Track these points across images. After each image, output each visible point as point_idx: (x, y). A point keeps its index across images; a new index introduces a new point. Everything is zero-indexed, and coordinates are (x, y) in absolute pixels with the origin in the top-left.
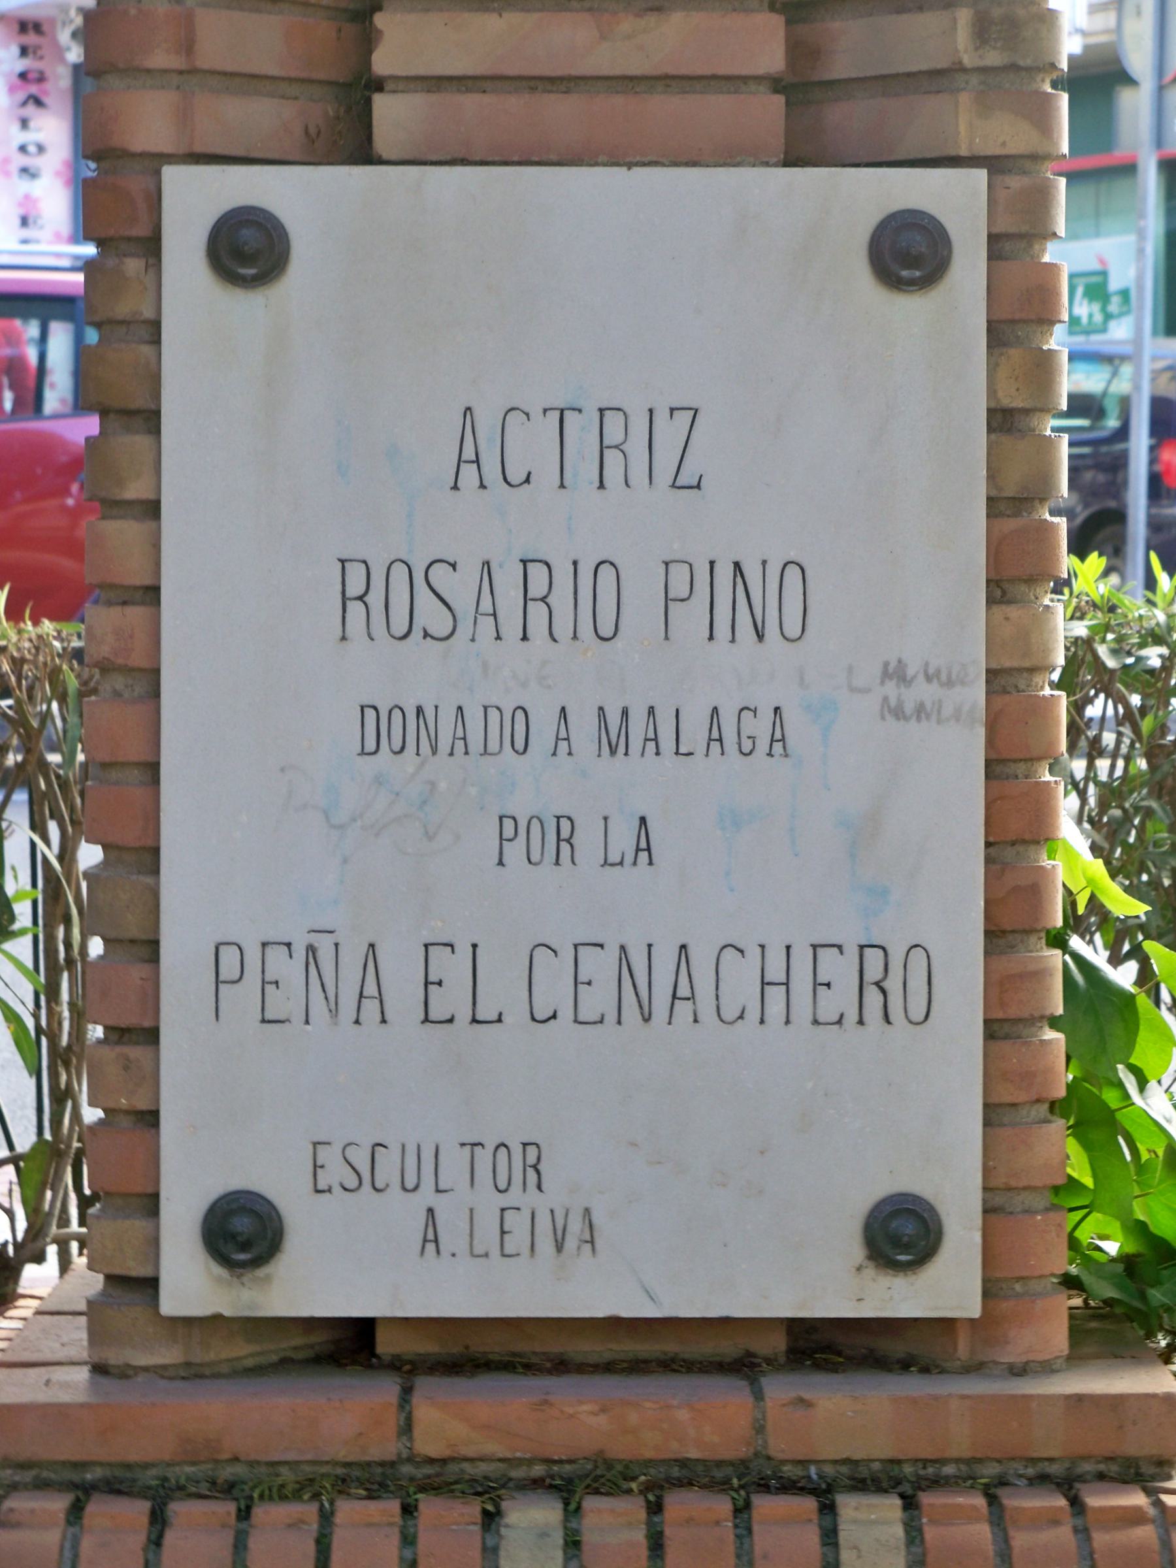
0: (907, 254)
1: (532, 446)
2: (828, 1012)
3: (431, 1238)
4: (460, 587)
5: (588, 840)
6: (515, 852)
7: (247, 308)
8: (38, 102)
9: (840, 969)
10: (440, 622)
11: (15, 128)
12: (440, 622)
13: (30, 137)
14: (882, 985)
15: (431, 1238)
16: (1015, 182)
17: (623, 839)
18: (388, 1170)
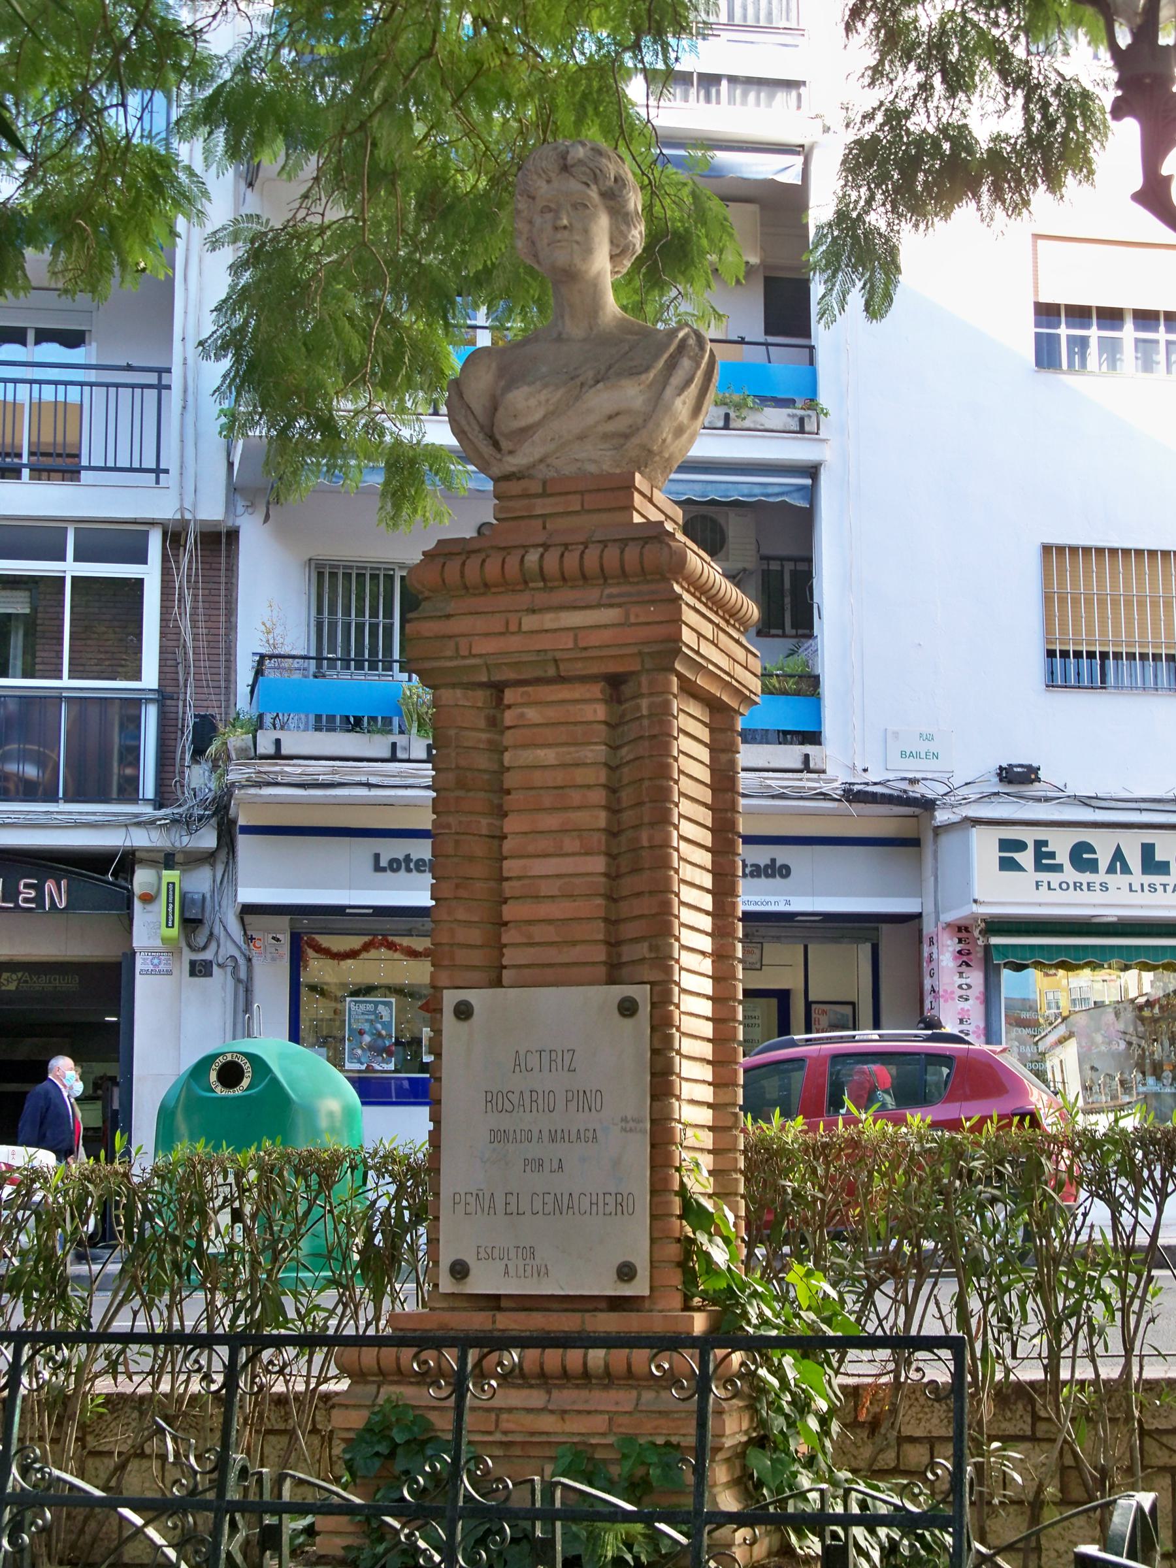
0: (627, 1008)
1: (533, 1061)
2: (608, 1210)
3: (507, 1273)
4: (515, 1098)
5: (547, 1165)
6: (528, 1168)
7: (464, 1026)
8: (968, 965)
9: (610, 1200)
10: (510, 1108)
11: (956, 977)
12: (510, 1108)
13: (963, 981)
14: (622, 1204)
15: (507, 1273)
16: (657, 988)
17: (555, 1165)
18: (496, 1254)
